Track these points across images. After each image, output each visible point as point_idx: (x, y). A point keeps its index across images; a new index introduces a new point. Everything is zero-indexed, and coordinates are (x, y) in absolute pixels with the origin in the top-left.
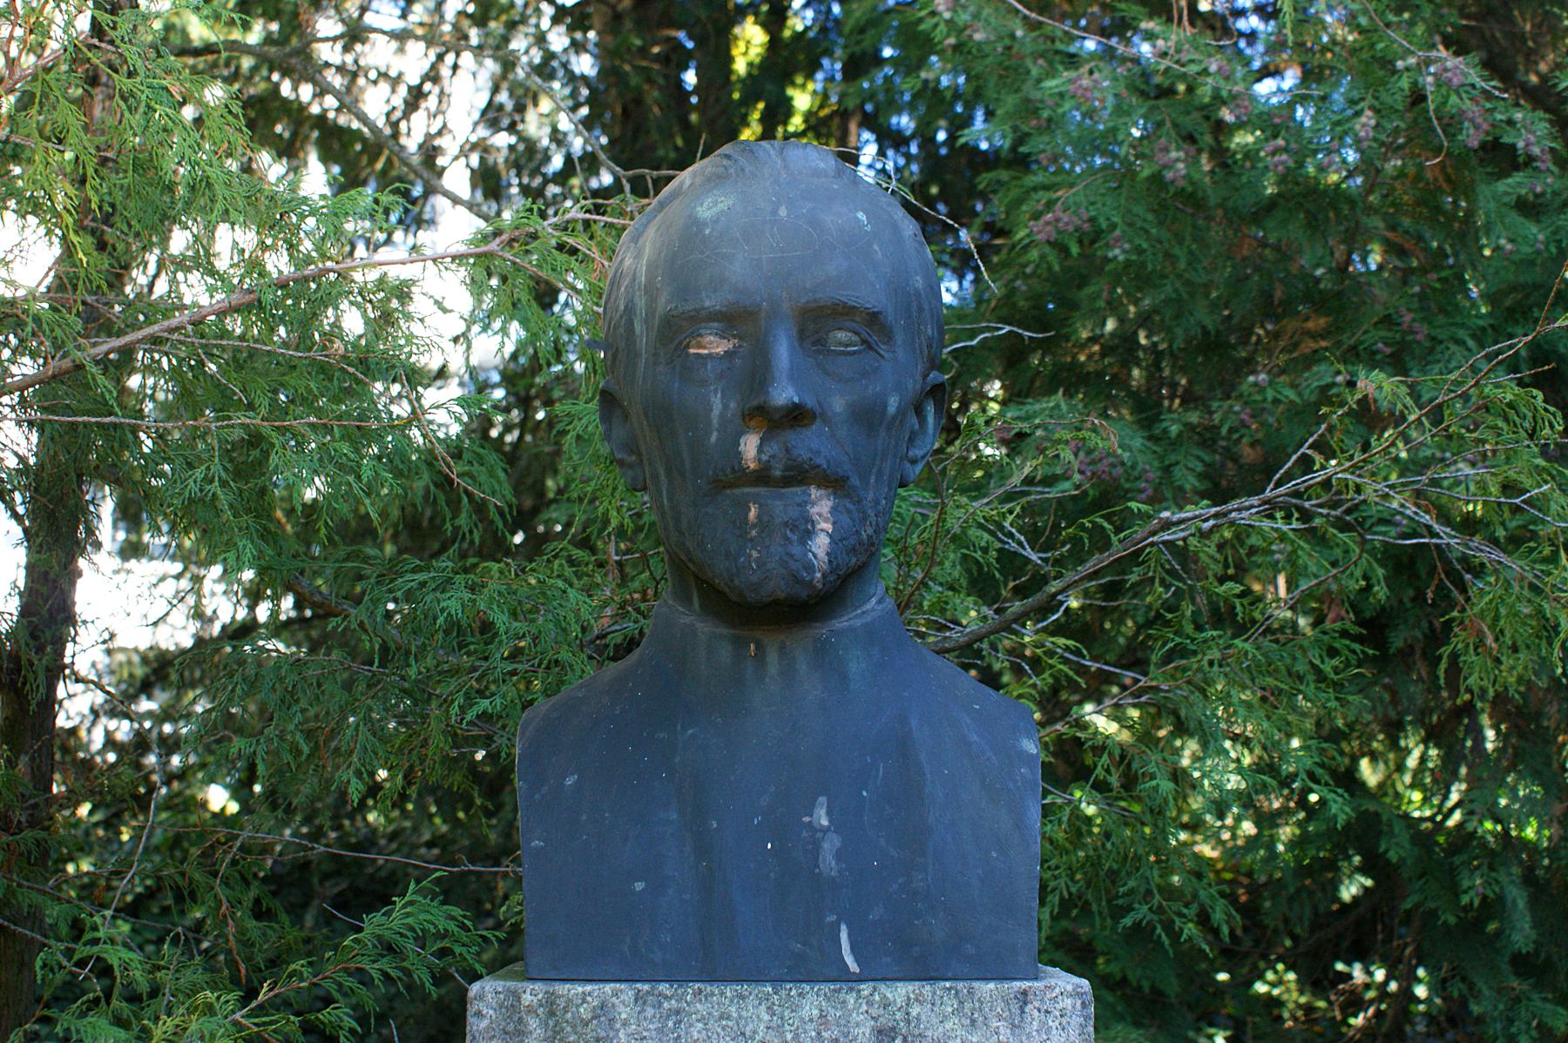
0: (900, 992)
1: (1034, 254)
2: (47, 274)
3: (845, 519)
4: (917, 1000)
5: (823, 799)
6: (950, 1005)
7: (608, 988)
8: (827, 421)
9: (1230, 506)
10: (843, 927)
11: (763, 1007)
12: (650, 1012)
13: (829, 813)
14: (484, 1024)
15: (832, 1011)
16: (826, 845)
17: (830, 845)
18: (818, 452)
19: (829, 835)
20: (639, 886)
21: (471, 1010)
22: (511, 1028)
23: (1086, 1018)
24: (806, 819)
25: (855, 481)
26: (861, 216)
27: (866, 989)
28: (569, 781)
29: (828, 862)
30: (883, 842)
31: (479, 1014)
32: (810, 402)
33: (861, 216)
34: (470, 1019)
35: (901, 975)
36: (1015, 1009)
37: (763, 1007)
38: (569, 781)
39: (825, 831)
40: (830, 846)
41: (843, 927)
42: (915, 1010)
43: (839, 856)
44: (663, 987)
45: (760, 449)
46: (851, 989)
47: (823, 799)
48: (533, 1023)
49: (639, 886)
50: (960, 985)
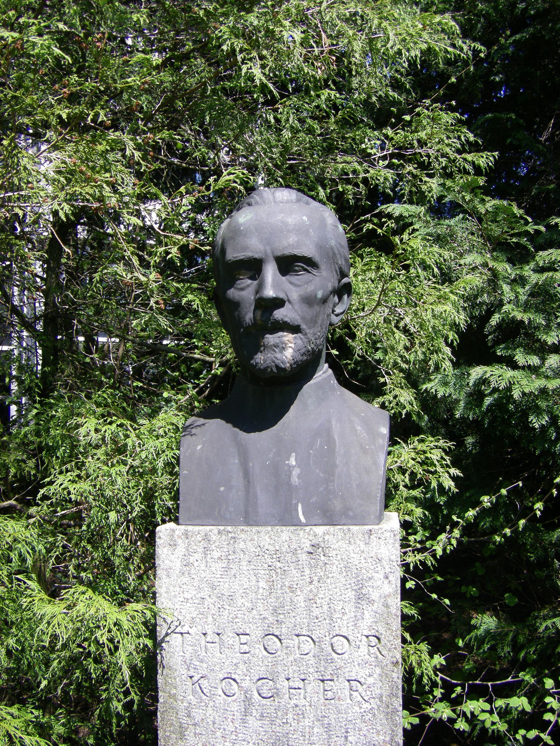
0: (320, 530)
1: (200, 260)
3: (299, 342)
5: (293, 454)
6: (340, 534)
7: (208, 528)
8: (290, 302)
10: (300, 505)
12: (224, 537)
13: (296, 460)
14: (162, 541)
16: (294, 472)
18: (286, 316)
20: (222, 489)
21: (157, 536)
23: (395, 540)
25: (303, 326)
26: (305, 218)
27: (308, 528)
28: (199, 447)
29: (295, 480)
30: (318, 471)
31: (160, 538)
32: (282, 295)
33: (305, 218)
34: (157, 540)
36: (367, 536)
38: (199, 447)
39: (294, 467)
40: (296, 472)
41: (300, 505)
42: (327, 537)
43: (299, 477)
44: (229, 528)
45: (262, 316)
47: (293, 454)
48: (180, 541)
49: (222, 489)
50: (345, 527)
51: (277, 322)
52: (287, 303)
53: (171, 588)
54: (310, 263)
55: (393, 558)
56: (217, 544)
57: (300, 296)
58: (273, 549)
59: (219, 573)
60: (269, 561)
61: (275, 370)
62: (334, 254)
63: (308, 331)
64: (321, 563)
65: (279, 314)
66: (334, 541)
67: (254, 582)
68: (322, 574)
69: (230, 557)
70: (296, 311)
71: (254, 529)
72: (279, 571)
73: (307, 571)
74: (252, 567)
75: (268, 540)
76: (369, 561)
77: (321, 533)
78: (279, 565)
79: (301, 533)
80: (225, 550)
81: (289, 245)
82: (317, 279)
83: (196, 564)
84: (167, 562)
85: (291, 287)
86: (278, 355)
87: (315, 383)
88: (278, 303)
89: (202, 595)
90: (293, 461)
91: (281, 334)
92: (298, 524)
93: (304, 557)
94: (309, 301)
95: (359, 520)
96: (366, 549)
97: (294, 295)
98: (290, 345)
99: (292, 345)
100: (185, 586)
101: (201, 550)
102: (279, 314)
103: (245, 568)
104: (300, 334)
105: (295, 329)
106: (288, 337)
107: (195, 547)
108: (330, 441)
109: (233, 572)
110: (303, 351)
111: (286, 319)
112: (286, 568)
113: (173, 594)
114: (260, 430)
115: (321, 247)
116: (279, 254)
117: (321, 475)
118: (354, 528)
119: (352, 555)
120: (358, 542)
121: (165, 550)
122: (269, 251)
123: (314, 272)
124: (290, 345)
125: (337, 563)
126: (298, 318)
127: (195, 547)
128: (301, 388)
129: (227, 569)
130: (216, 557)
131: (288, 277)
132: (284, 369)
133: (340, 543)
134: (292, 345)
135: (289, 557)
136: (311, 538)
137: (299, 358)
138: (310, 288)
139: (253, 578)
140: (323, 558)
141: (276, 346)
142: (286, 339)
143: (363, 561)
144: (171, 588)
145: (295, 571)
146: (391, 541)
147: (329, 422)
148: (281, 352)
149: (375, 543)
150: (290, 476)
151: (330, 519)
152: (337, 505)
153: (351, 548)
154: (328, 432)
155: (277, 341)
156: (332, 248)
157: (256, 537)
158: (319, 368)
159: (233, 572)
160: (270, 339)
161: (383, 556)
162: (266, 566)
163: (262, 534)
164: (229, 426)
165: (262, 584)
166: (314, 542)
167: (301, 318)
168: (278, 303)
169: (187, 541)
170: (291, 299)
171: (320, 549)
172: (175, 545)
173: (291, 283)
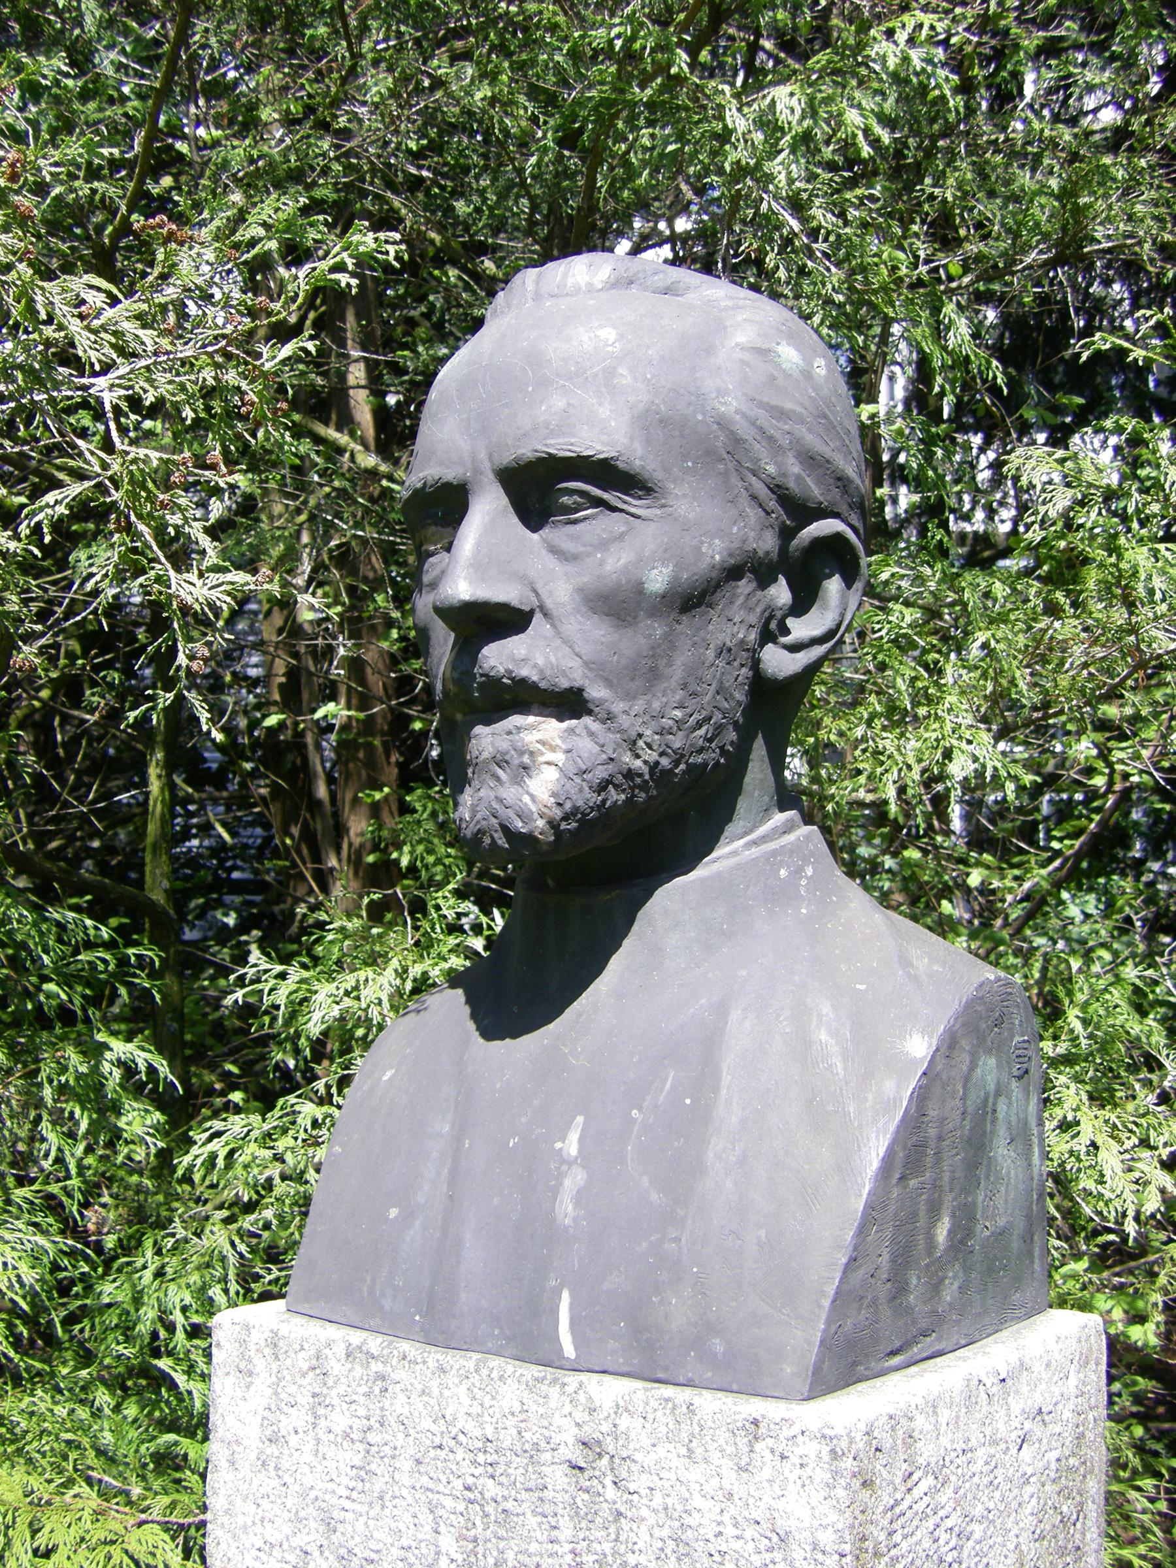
0: (609, 1391)
2: (585, 519)
3: (586, 746)
4: (627, 1410)
6: (664, 1419)
9: (319, 768)
10: (566, 1296)
11: (464, 1387)
12: (358, 1371)
13: (582, 1140)
15: (533, 1407)
17: (573, 1181)
19: (575, 1168)
22: (242, 1365)
23: (836, 1474)
24: (558, 1145)
25: (596, 692)
30: (645, 1181)
35: (625, 1369)
36: (742, 1442)
37: (464, 1387)
39: (570, 1163)
40: (573, 1181)
41: (566, 1296)
42: (624, 1422)
44: (375, 1343)
46: (555, 1381)
47: (580, 1119)
48: (260, 1364)
50: (682, 1395)
51: (493, 683)
52: (537, 618)
53: (239, 1501)
54: (611, 479)
55: (826, 1538)
56: (342, 1389)
57: (580, 590)
58: (478, 1433)
59: (345, 1481)
60: (466, 1468)
61: (502, 842)
62: (737, 441)
63: (618, 707)
64: (605, 1511)
65: (499, 657)
66: (646, 1442)
67: (426, 1532)
68: (607, 1547)
69: (372, 1437)
70: (567, 642)
71: (436, 1356)
72: (490, 1509)
73: (566, 1524)
74: (425, 1480)
75: (466, 1401)
76: (750, 1532)
77: (608, 1406)
78: (492, 1489)
79: (554, 1391)
80: (362, 1412)
81: (535, 428)
82: (651, 529)
83: (293, 1440)
84: (230, 1420)
85: (552, 562)
86: (509, 793)
87: (703, 880)
88: (504, 621)
89: (300, 1540)
90: (571, 1145)
91: (516, 720)
92: (551, 1359)
93: (558, 1477)
94: (617, 604)
95: (741, 1375)
96: (739, 1490)
97: (559, 588)
98: (549, 756)
99: (559, 758)
100: (265, 1504)
101: (305, 1400)
102: (499, 657)
103: (407, 1481)
104: (587, 720)
105: (569, 704)
106: (540, 732)
107: (292, 1389)
108: (705, 1080)
109: (378, 1485)
110: (601, 773)
111: (524, 672)
112: (509, 1505)
113: (241, 1520)
114: (514, 1036)
115: (663, 422)
116: (506, 458)
117: (654, 1197)
118: (709, 1402)
119: (697, 1501)
120: (715, 1456)
121: (231, 1379)
122: (483, 455)
123: (635, 505)
124: (549, 756)
125: (652, 1520)
126: (576, 663)
127: (292, 1389)
128: (649, 895)
129: (363, 1472)
130: (338, 1430)
131: (546, 532)
132: (528, 840)
133: (661, 1451)
134: (559, 758)
135: (517, 1468)
136: (580, 1416)
137: (584, 797)
138: (614, 564)
139: (426, 1519)
140: (611, 1492)
141: (501, 761)
142: (530, 739)
143: (730, 1531)
144: (239, 1501)
145: (533, 1521)
146: (822, 1475)
147: (722, 1010)
148: (518, 781)
149: (767, 1473)
150: (555, 1192)
151: (652, 1360)
152: (677, 1311)
153: (695, 1474)
154: (710, 1043)
155: (504, 744)
156: (722, 423)
157: (434, 1385)
158: (730, 829)
159: (378, 1485)
160: (486, 739)
161: (792, 1524)
162: (458, 1485)
163: (451, 1379)
164: (467, 1010)
165: (448, 1543)
166: (588, 1432)
167: (586, 664)
168: (504, 621)
169: (274, 1366)
170: (549, 604)
171: (605, 1460)
172: (250, 1374)
173: (554, 551)
